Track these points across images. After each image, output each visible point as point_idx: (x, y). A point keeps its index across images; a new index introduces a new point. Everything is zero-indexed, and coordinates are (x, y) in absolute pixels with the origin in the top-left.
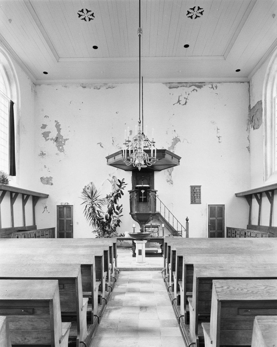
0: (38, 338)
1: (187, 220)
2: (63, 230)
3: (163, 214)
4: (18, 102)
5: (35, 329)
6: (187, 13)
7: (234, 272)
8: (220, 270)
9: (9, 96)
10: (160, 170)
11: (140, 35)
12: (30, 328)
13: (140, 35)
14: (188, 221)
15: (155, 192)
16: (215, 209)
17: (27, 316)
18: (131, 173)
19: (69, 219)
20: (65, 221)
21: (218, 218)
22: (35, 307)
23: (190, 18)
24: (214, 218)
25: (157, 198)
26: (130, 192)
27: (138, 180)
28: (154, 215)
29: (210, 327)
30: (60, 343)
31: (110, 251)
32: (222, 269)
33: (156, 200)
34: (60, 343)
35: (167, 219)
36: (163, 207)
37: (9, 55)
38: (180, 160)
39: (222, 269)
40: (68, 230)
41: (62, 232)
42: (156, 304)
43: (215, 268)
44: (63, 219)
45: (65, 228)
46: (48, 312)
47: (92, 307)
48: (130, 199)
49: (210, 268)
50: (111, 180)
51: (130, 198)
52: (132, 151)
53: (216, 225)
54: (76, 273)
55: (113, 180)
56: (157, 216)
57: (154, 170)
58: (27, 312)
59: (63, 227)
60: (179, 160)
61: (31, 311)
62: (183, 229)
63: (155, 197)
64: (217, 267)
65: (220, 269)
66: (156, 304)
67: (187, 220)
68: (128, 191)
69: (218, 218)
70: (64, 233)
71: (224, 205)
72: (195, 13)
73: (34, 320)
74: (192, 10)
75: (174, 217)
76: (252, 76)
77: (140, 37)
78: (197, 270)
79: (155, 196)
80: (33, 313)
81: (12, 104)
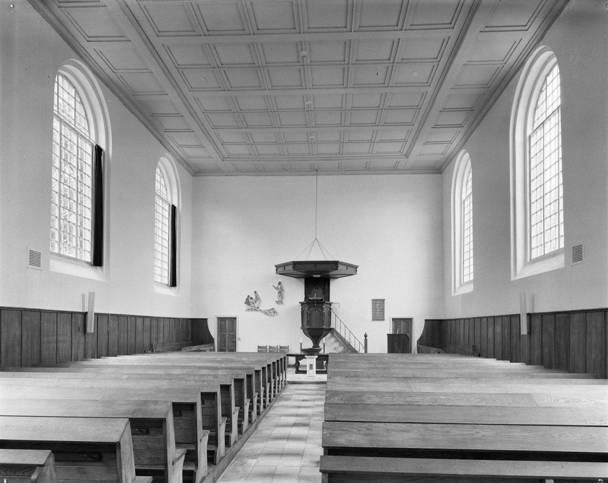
0: (151, 458)
1: (366, 336)
3: (338, 330)
5: (149, 449)
7: (391, 438)
8: (366, 435)
9: (93, 138)
12: (143, 448)
15: (330, 304)
17: (141, 437)
18: (303, 280)
22: (150, 427)
26: (302, 304)
29: (401, 353)
30: (173, 465)
31: (268, 368)
32: (370, 432)
33: (330, 312)
34: (173, 465)
35: (342, 334)
38: (358, 269)
39: (370, 432)
43: (359, 430)
45: (227, 346)
46: (161, 433)
49: (348, 431)
50: (276, 286)
51: (301, 310)
54: (164, 410)
55: (279, 286)
58: (141, 431)
61: (145, 430)
62: (361, 347)
64: (362, 429)
65: (367, 432)
67: (366, 336)
68: (300, 303)
73: (147, 440)
78: (325, 434)
79: (330, 309)
80: (147, 433)
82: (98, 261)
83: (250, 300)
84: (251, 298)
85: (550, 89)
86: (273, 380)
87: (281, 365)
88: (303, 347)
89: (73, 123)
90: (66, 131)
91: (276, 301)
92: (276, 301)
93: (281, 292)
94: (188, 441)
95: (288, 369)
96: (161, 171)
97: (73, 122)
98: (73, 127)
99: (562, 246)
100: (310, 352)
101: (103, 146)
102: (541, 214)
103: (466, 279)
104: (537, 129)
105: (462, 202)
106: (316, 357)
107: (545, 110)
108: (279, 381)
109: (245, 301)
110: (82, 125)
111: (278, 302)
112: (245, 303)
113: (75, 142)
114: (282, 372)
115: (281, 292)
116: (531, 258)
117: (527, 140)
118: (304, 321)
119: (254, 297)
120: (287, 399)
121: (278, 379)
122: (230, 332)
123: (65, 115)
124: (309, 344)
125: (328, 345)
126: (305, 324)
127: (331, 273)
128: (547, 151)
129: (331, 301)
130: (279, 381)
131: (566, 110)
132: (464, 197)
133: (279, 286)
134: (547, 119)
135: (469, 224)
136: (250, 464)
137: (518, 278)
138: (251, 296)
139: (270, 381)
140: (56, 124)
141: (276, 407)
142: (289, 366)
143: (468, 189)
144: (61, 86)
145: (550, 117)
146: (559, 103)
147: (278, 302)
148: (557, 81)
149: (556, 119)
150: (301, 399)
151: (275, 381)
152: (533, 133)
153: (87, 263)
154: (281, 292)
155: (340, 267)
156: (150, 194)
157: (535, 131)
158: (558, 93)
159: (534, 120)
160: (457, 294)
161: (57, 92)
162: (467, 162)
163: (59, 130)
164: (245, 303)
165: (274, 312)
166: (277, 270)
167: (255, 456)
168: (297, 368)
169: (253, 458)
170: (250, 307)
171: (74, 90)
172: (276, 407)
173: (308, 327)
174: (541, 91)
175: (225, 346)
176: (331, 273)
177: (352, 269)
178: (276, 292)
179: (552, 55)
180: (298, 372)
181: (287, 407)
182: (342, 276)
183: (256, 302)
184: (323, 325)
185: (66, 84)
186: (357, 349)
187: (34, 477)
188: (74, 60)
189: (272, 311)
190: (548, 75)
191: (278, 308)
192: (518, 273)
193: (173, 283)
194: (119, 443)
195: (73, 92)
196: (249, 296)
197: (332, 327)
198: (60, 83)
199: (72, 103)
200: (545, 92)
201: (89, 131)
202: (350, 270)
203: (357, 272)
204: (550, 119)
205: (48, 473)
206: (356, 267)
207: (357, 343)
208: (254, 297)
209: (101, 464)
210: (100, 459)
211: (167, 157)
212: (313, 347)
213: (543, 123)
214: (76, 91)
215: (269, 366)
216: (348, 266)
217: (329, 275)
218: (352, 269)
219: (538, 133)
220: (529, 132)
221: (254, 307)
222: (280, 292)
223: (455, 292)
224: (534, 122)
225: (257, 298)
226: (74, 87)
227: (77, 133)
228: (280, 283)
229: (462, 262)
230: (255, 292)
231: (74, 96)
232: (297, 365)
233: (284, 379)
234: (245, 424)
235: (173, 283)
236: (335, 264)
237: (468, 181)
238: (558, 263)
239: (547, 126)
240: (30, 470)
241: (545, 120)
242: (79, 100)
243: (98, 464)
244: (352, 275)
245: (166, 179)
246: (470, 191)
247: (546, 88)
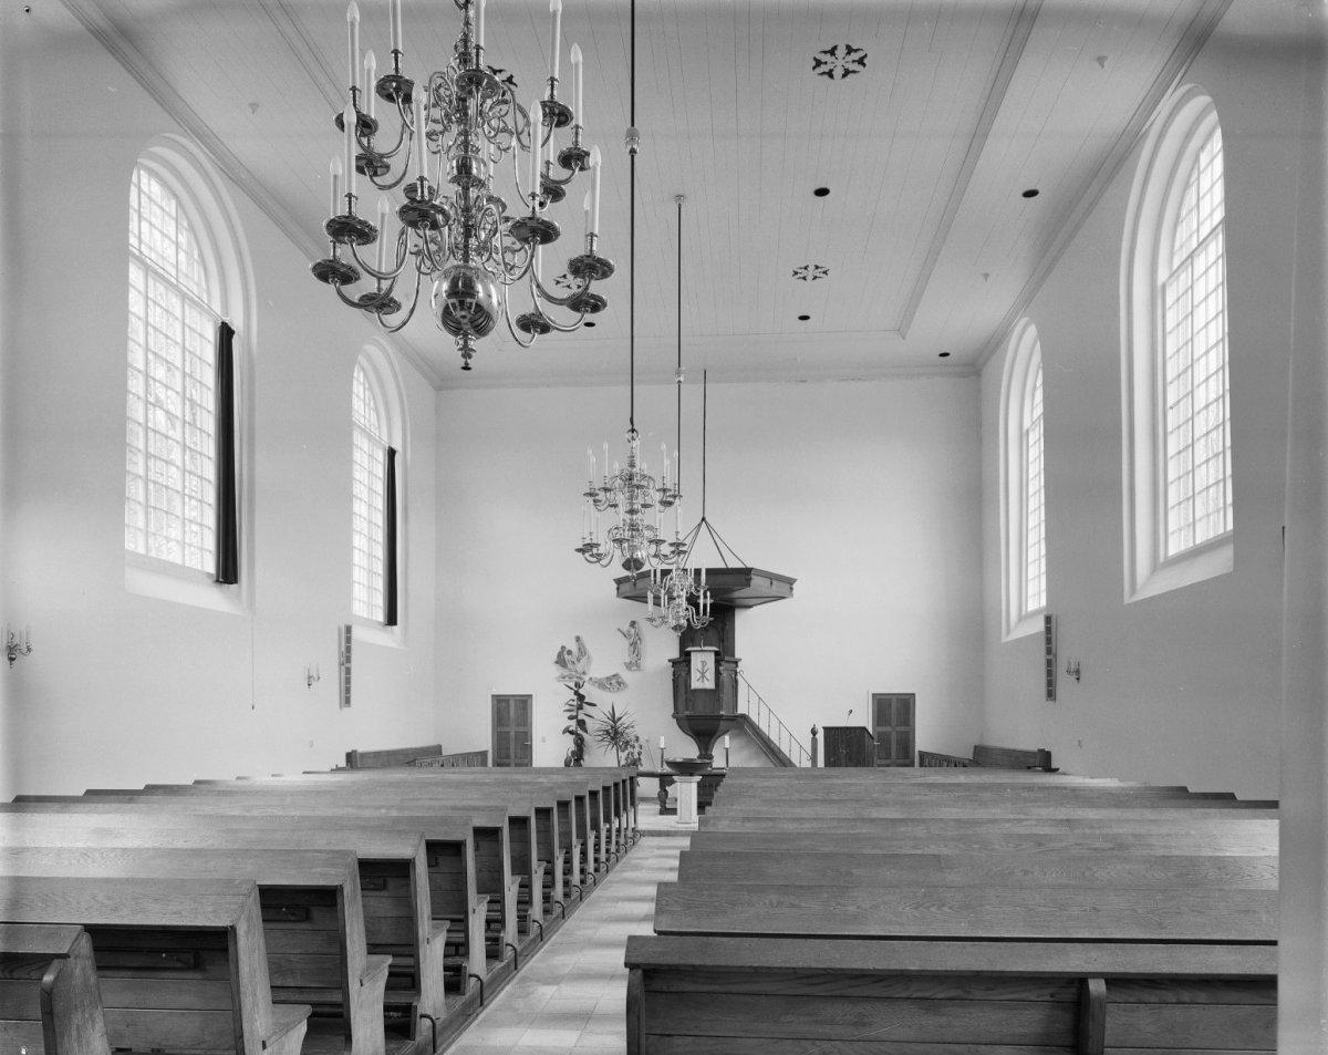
3: (754, 718)
4: (404, 447)
6: (814, 63)
10: (750, 607)
11: (633, 152)
13: (633, 152)
15: (736, 663)
16: (890, 705)
19: (522, 729)
20: (512, 734)
21: (898, 729)
23: (826, 77)
24: (888, 729)
25: (739, 677)
28: (733, 720)
30: (947, 354)
33: (736, 681)
36: (754, 699)
38: (794, 586)
45: (512, 755)
48: (673, 680)
53: (894, 746)
56: (742, 724)
59: (508, 749)
60: (792, 584)
62: (804, 756)
63: (736, 675)
69: (898, 729)
71: (914, 695)
72: (839, 63)
74: (829, 55)
76: (985, 363)
77: (633, 157)
79: (736, 672)
81: (392, 453)
82: (228, 571)
83: (566, 656)
84: (570, 652)
85: (1205, 183)
86: (604, 827)
87: (625, 793)
88: (670, 756)
89: (174, 273)
90: (157, 290)
91: (625, 664)
92: (625, 664)
93: (635, 645)
94: (398, 947)
95: (641, 807)
96: (365, 376)
97: (174, 272)
98: (175, 282)
99: (1230, 527)
100: (686, 768)
101: (237, 324)
102: (1218, 465)
103: (1032, 606)
104: (1179, 268)
105: (1023, 435)
106: (699, 778)
107: (1195, 226)
108: (618, 830)
109: (555, 658)
110: (193, 281)
111: (629, 666)
112: (557, 662)
113: (178, 313)
114: (625, 809)
116: (1166, 553)
117: (1156, 294)
118: (680, 702)
119: (575, 650)
120: (636, 868)
121: (616, 824)
122: (518, 725)
123: (153, 256)
124: (688, 750)
125: (727, 753)
126: (681, 708)
127: (737, 594)
128: (1200, 318)
129: (737, 656)
130: (618, 830)
131: (1236, 227)
132: (1027, 424)
133: (633, 630)
134: (1199, 245)
135: (1037, 483)
136: (543, 994)
137: (1139, 597)
138: (568, 648)
139: (595, 827)
140: (135, 274)
141: (611, 882)
142: (645, 800)
143: (1035, 408)
144: (145, 193)
145: (1207, 242)
146: (1219, 215)
147: (629, 666)
148: (1218, 165)
149: (1217, 247)
150: (667, 866)
151: (609, 831)
152: (1170, 277)
153: (379, 623)
154: (635, 645)
155: (756, 581)
156: (340, 432)
157: (1173, 274)
158: (1219, 193)
159: (1173, 247)
160: (1014, 637)
161: (136, 208)
162: (1034, 346)
163: (142, 289)
164: (557, 662)
165: (619, 684)
166: (618, 589)
167: (554, 979)
168: (663, 803)
169: (549, 984)
170: (566, 672)
171: (173, 202)
172: (611, 882)
173: (687, 713)
174: (1187, 186)
175: (508, 757)
176: (737, 594)
177: (782, 586)
178: (625, 643)
179: (1209, 104)
180: (665, 811)
181: (634, 882)
182: (759, 601)
183: (579, 660)
184: (721, 708)
185: (155, 189)
186: (795, 760)
187: (48, 978)
188: (172, 136)
189: (613, 682)
190: (1202, 148)
191: (626, 676)
192: (1138, 587)
193: (392, 619)
194: (233, 928)
195: (172, 207)
196: (563, 648)
197: (741, 710)
198: (144, 187)
199: (171, 229)
200: (1194, 188)
201: (209, 295)
202: (776, 589)
203: (794, 591)
204: (1207, 245)
205: (78, 971)
206: (790, 582)
207: (795, 747)
208: (575, 650)
209: (198, 975)
210: (197, 966)
211: (380, 346)
212: (699, 758)
213: (1191, 256)
214: (180, 204)
215: (593, 794)
216: (773, 578)
217: (732, 600)
218: (782, 586)
219: (1181, 278)
220: (1162, 276)
221: (576, 671)
222: (634, 644)
223: (1008, 632)
224: (1172, 254)
225: (582, 651)
226: (175, 196)
227: (184, 297)
228: (633, 624)
229: (1022, 569)
230: (578, 639)
231: (174, 215)
232: (663, 797)
233: (632, 825)
234: (536, 911)
235: (392, 619)
236: (744, 575)
237: (1034, 388)
238: (1221, 562)
239: (1200, 263)
240: (41, 968)
241: (1196, 250)
242: (185, 224)
243: (190, 975)
244: (784, 598)
245: (203, 234)
246: (1039, 410)
247: (1198, 178)
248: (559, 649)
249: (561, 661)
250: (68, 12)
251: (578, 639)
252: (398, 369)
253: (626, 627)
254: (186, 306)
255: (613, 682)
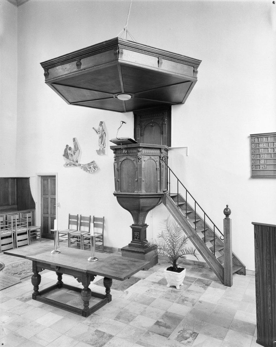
1: (227, 213)
2: (48, 213)
14: (230, 217)
18: (131, 114)
27: (144, 127)
37: (165, 174)
40: (52, 213)
41: (46, 215)
42: (132, 1)
44: (47, 196)
47: (167, 87)
50: (97, 128)
52: (175, 344)
55: (101, 128)
57: (170, 104)
66: (132, 1)
67: (227, 213)
70: (48, 217)
75: (187, 192)
84: (70, 149)
91: (97, 151)
92: (97, 151)
109: (63, 153)
115: (103, 136)
119: (72, 147)
133: (101, 128)
138: (70, 146)
178: (98, 136)
184: (139, 188)
196: (67, 146)
208: (72, 147)
221: (73, 160)
225: (77, 148)
248: (65, 147)
249: (66, 155)
250: (177, 224)
251: (74, 140)
252: (124, 140)
253: (97, 127)
254: (221, 226)
255: (92, 166)
